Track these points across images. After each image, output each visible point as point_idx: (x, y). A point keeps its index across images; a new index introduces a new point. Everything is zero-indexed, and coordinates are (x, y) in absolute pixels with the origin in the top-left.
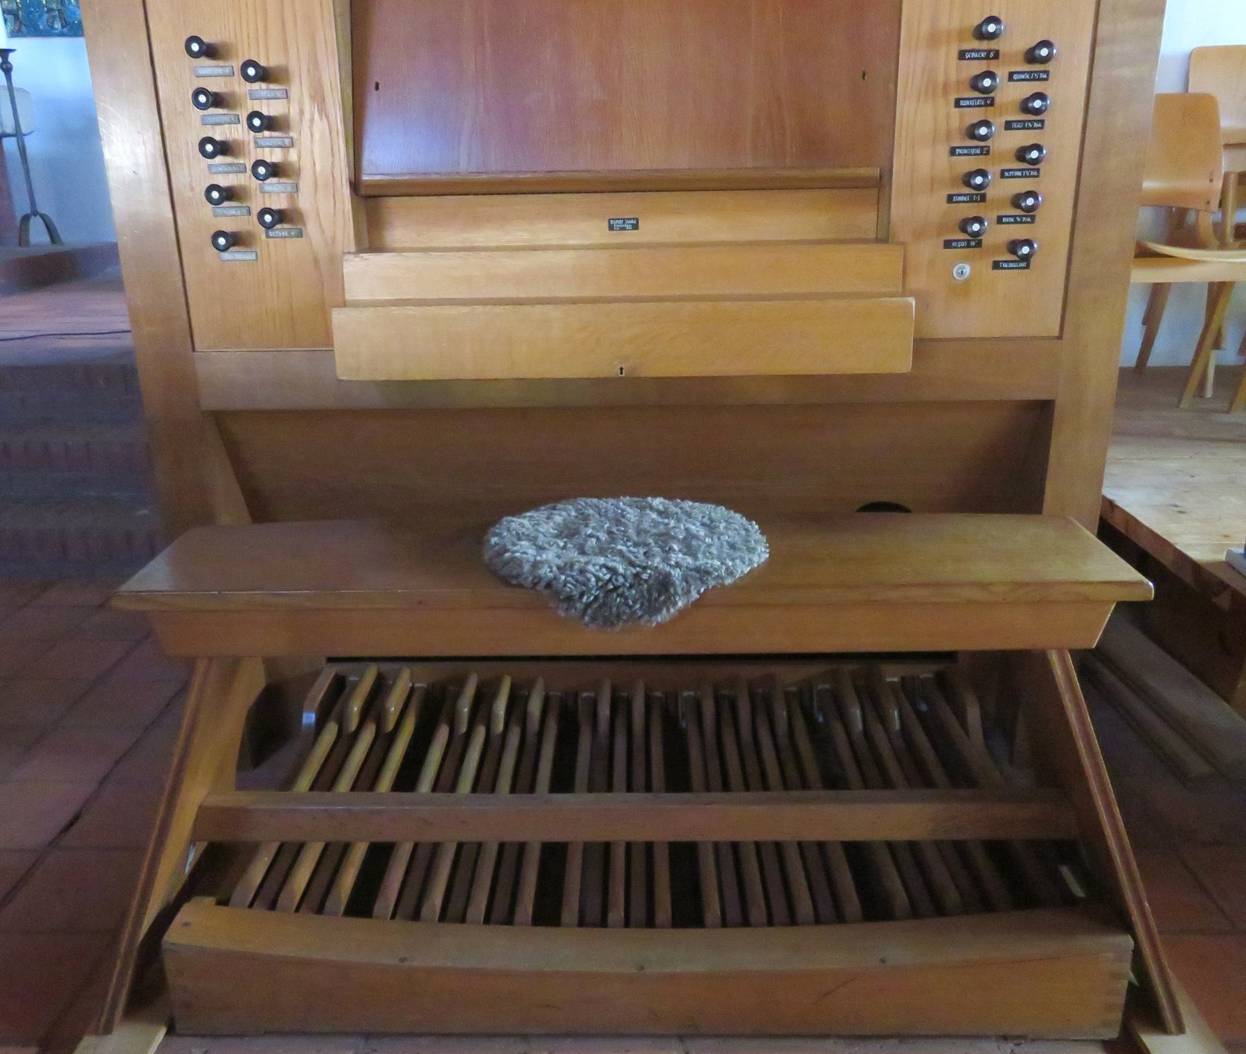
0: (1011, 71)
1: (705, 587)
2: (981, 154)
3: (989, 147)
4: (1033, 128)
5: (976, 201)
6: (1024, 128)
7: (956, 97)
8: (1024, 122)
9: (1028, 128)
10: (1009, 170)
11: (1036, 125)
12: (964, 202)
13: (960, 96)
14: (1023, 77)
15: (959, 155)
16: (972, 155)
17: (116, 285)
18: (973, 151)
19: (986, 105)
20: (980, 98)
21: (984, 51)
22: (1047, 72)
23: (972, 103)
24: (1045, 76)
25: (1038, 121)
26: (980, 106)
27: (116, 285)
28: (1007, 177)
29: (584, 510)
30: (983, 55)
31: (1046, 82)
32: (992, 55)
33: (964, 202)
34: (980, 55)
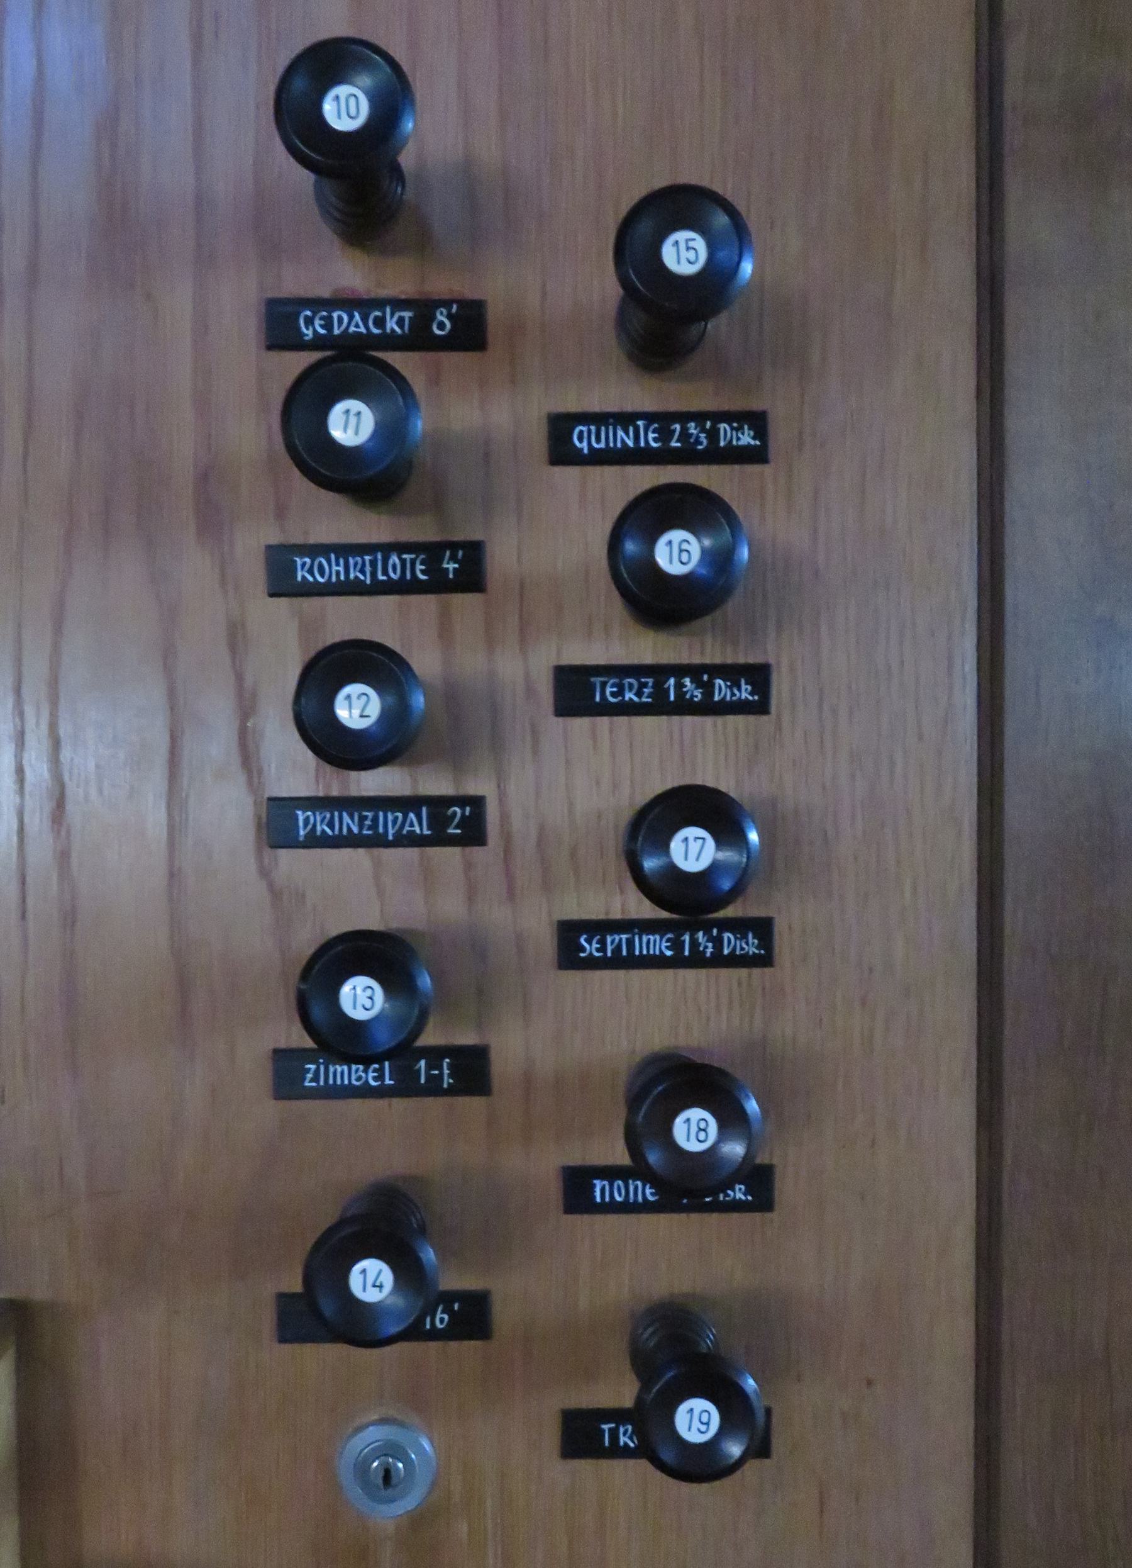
0: (561, 409)
1: (700, 435)
2: (439, 839)
3: (477, 803)
4: (709, 708)
5: (433, 1089)
6: (659, 707)
7: (275, 539)
8: (659, 672)
9: (684, 707)
10: (600, 928)
11: (721, 689)
12: (364, 1092)
13: (572, 405)
14: (624, 438)
15: (315, 841)
16: (388, 844)
17: (354, 415)
18: (390, 823)
19: (438, 584)
20: (401, 548)
21: (398, 304)
22: (758, 421)
23: (357, 570)
24: (746, 438)
25: (733, 673)
26: (404, 587)
27: (354, 415)
28: (592, 964)
29: (921, 157)
30: (391, 324)
31: (697, 836)
32: (442, 323)
33: (364, 1092)
34: (380, 322)
